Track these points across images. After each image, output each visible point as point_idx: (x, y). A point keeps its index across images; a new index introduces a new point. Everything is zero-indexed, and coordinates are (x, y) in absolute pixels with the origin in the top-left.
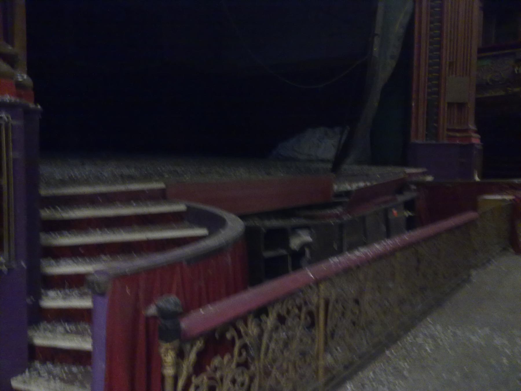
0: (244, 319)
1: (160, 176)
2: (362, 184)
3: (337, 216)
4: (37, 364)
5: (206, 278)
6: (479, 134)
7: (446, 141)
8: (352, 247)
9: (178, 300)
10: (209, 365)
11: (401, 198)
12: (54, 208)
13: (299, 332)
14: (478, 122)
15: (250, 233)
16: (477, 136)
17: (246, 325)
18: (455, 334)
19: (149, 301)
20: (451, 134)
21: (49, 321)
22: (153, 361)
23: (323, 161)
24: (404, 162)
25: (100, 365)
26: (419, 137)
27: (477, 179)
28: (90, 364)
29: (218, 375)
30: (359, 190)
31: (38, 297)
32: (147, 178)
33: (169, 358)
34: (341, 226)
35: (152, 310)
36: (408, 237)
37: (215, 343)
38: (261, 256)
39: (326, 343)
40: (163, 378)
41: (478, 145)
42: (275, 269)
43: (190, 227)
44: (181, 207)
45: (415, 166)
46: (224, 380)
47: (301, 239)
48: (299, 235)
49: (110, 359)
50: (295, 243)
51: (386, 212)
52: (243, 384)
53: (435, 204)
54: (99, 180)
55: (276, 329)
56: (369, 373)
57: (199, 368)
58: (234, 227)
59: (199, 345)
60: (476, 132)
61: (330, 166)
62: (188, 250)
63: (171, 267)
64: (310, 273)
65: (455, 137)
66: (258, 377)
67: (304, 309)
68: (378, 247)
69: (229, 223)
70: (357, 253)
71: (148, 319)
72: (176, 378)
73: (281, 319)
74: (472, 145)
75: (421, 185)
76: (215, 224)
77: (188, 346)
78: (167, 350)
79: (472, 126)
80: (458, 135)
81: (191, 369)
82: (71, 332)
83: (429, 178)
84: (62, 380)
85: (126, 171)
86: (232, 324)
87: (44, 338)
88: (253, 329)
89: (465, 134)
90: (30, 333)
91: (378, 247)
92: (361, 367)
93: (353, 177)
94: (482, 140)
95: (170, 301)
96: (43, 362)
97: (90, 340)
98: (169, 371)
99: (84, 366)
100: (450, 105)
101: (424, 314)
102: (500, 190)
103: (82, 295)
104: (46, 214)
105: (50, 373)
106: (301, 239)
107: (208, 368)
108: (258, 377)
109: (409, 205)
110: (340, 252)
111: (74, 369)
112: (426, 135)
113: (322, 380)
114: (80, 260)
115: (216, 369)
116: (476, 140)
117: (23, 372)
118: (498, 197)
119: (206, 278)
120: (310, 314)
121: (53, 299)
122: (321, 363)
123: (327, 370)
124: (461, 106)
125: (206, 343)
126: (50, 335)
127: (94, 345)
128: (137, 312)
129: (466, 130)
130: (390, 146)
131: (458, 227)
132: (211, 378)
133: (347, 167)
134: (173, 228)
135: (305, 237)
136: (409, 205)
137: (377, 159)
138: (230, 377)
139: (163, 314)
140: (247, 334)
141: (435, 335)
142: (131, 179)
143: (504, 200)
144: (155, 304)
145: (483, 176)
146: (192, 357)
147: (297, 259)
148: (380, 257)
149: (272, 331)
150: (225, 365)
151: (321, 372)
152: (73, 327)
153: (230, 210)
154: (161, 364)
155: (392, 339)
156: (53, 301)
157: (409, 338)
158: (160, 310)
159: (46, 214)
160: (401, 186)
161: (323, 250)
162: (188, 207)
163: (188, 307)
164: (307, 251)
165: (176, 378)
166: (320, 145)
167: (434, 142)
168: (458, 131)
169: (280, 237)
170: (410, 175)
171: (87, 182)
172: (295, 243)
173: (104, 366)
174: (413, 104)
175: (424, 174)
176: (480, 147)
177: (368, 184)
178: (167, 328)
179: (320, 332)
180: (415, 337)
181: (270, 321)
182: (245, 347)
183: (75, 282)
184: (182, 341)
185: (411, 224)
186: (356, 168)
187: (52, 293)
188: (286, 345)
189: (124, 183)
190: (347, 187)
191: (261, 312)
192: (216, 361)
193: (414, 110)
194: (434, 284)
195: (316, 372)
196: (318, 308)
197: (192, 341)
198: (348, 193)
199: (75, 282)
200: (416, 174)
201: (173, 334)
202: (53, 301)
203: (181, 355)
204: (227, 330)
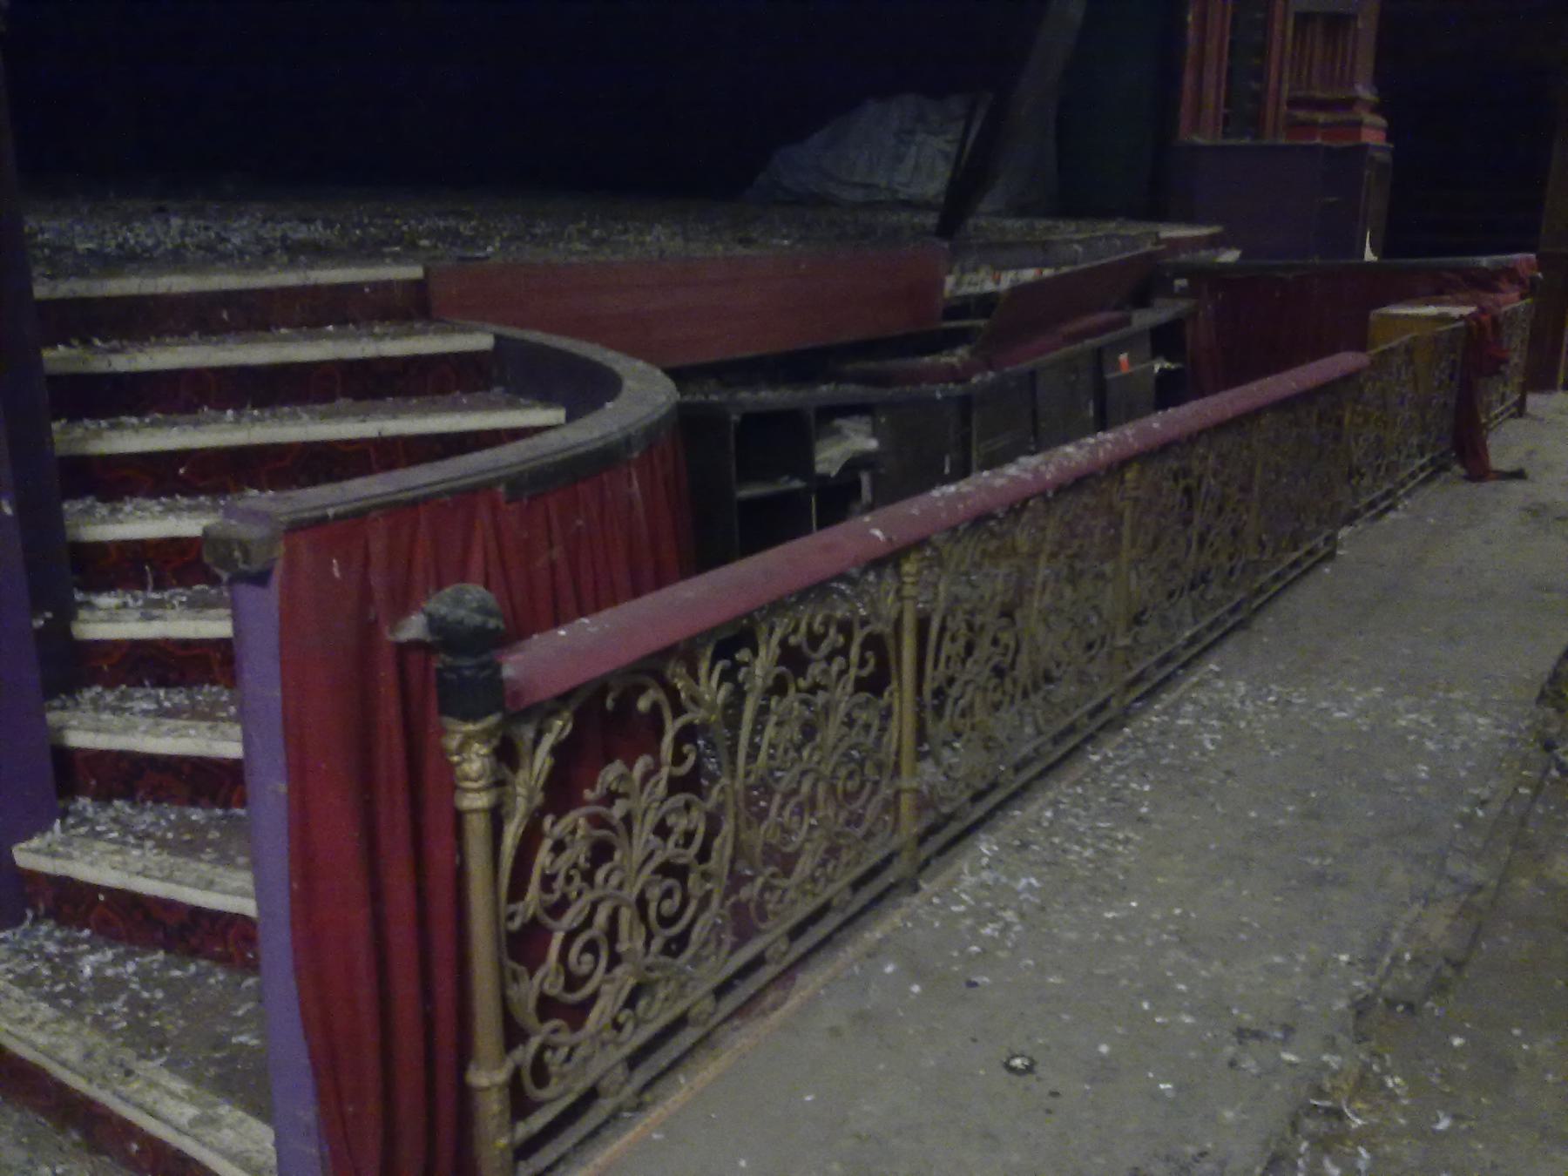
0: (686, 652)
1: (409, 249)
2: (1029, 275)
3: (954, 375)
4: (84, 803)
5: (565, 536)
6: (1384, 116)
7: (1283, 141)
8: (994, 461)
9: (491, 599)
10: (593, 788)
11: (1144, 319)
12: (86, 342)
13: (843, 697)
14: (1380, 80)
15: (689, 425)
16: (1381, 121)
17: (693, 674)
18: (1284, 704)
19: (403, 605)
20: (1301, 114)
21: (110, 685)
22: (425, 776)
23: (908, 204)
24: (1159, 213)
25: (271, 790)
26: (1201, 132)
27: (1369, 256)
28: (243, 803)
29: (618, 811)
30: (1019, 291)
31: (67, 613)
32: (369, 251)
33: (475, 762)
34: (966, 404)
35: (414, 628)
36: (1158, 424)
37: (606, 722)
38: (728, 480)
39: (921, 735)
40: (459, 817)
41: (1381, 149)
42: (771, 524)
43: (511, 405)
44: (481, 341)
45: (1190, 219)
46: (636, 829)
47: (845, 445)
48: (837, 432)
49: (299, 773)
50: (830, 457)
51: (1099, 360)
52: (689, 836)
53: (1247, 327)
54: (214, 255)
55: (779, 687)
56: (1038, 810)
57: (561, 792)
58: (644, 395)
59: (560, 727)
60: (1376, 109)
61: (932, 220)
62: (509, 454)
63: (468, 496)
64: (873, 529)
65: (1314, 124)
66: (730, 812)
67: (859, 636)
68: (1074, 455)
69: (629, 384)
70: (1012, 470)
71: (404, 649)
72: (497, 818)
73: (793, 660)
74: (1366, 147)
75: (1207, 278)
76: (585, 388)
77: (528, 733)
78: (468, 739)
79: (1365, 92)
80: (1321, 117)
81: (539, 798)
82: (174, 713)
83: (1230, 256)
84: (162, 844)
85: (302, 233)
86: (652, 668)
87: (91, 729)
88: (712, 690)
89: (1343, 116)
90: (53, 718)
91: (1074, 455)
92: (1018, 795)
93: (998, 253)
94: (1391, 135)
95: (467, 601)
96: (103, 797)
97: (244, 879)
98: (475, 801)
99: (226, 805)
100: (1304, 19)
101: (1200, 648)
102: (1437, 292)
103: (198, 605)
104: (59, 357)
105: (126, 828)
106: (845, 445)
107: (588, 794)
108: (730, 812)
109: (1165, 339)
110: (962, 471)
111: (196, 815)
112: (1226, 119)
113: (910, 827)
114: (184, 501)
115: (610, 798)
116: (1373, 133)
117: (43, 827)
118: (1432, 310)
119: (565, 536)
120: (874, 643)
121: (112, 616)
122: (906, 782)
123: (924, 803)
124: (1337, 23)
125: (579, 718)
126: (117, 721)
127: (247, 742)
128: (368, 632)
129: (1349, 104)
130: (1115, 158)
131: (1306, 397)
132: (597, 821)
133: (986, 218)
134: (455, 408)
135: (859, 439)
136: (1165, 339)
137: (1074, 200)
138: (651, 819)
139: (447, 637)
140: (695, 700)
141: (1227, 704)
142: (320, 253)
143: (1442, 319)
144: (423, 611)
145: (1384, 250)
146: (542, 760)
147: (837, 498)
148: (1079, 482)
149: (769, 692)
150: (636, 786)
151: (906, 802)
152: (179, 698)
153: (634, 351)
154: (451, 783)
155: (1106, 721)
156: (111, 620)
157: (1154, 717)
158: (436, 624)
159: (59, 357)
160: (1145, 280)
161: (906, 472)
162: (498, 338)
163: (515, 632)
164: (865, 478)
165: (497, 818)
166: (906, 155)
167: (1246, 141)
168: (1322, 105)
169: (786, 437)
170: (1175, 244)
171: (177, 260)
172: (830, 457)
173: (283, 788)
174: (1190, 18)
175: (1214, 243)
176: (1384, 157)
177: (1047, 272)
178: (460, 675)
179: (902, 696)
180: (1175, 710)
181: (762, 666)
182: (687, 734)
183: (169, 566)
184: (510, 715)
185: (1168, 392)
186: (1014, 225)
187: (106, 601)
188: (809, 731)
189: (292, 264)
190: (984, 282)
191: (733, 641)
192: (611, 774)
193: (1191, 34)
194: (1235, 555)
195: (892, 804)
196: (898, 624)
197: (541, 713)
198: (986, 303)
199: (169, 566)
200: (1196, 243)
201: (478, 694)
202: (111, 620)
203: (507, 755)
204: (641, 689)
